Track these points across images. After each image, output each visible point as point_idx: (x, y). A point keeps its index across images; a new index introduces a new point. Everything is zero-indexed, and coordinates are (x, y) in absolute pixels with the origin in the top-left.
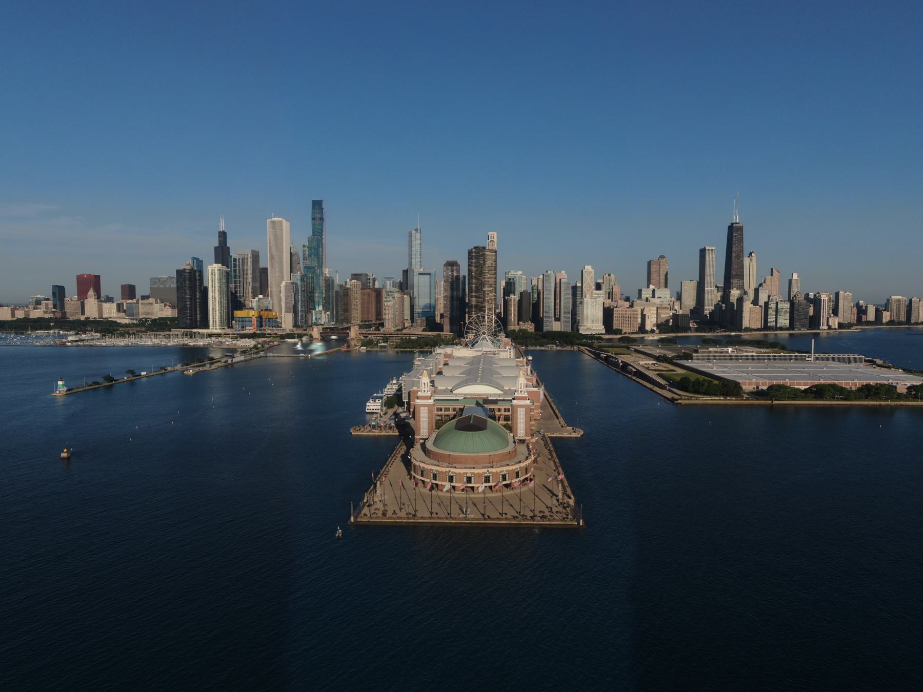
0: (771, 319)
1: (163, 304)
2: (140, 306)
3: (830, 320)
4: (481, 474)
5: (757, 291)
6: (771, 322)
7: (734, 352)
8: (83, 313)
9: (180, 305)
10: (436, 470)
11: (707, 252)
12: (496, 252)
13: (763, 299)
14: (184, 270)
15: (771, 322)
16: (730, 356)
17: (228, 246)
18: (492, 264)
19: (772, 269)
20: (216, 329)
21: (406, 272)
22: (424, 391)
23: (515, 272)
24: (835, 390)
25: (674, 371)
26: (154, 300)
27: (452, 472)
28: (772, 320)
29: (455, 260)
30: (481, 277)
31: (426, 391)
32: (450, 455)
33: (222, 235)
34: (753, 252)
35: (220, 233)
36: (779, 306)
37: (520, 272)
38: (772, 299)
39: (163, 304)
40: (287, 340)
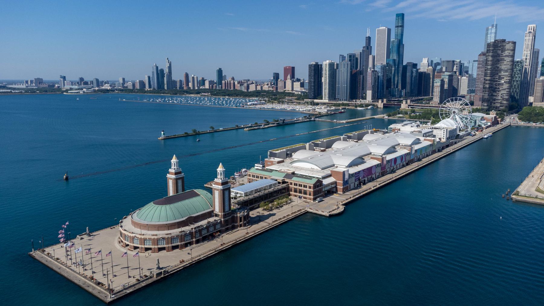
12: (514, 43)
17: (403, 43)
18: (509, 53)
20: (326, 100)
30: (498, 64)
33: (368, 39)
35: (366, 38)
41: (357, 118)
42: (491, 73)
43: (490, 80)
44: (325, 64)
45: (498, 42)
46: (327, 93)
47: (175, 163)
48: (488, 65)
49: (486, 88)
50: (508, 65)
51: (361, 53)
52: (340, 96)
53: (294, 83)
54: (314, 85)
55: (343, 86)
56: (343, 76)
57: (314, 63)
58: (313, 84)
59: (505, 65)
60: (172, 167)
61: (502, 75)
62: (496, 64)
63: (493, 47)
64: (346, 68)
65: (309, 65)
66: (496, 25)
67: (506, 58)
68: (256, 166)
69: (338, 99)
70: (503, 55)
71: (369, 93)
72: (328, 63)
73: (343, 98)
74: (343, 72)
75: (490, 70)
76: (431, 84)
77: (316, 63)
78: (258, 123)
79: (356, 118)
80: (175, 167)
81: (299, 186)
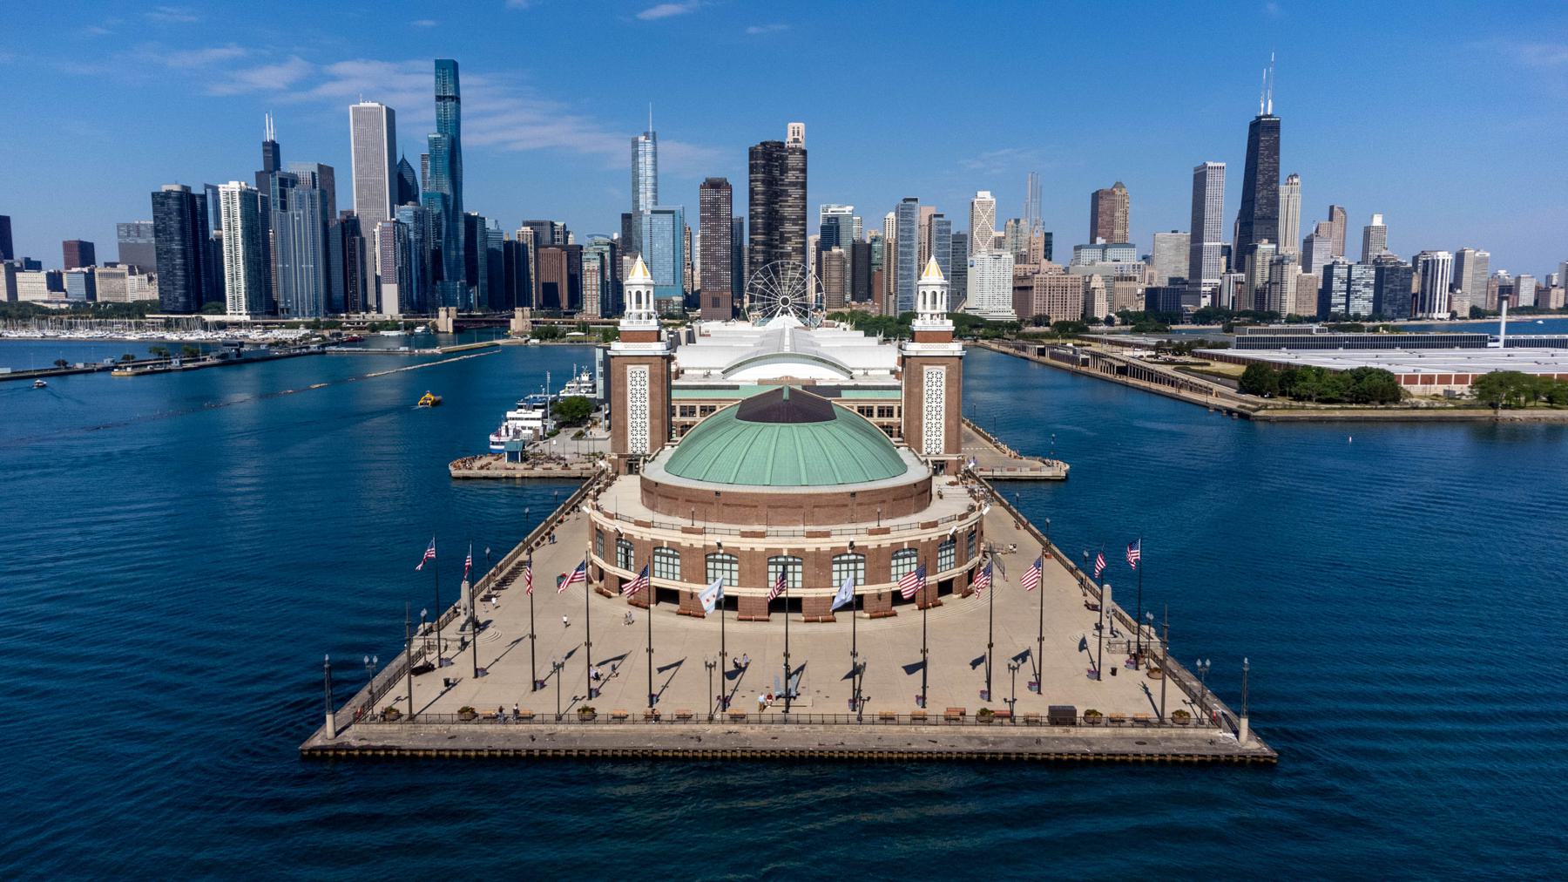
0: (1337, 299)
1: (145, 277)
2: (97, 279)
4: (826, 554)
5: (1308, 244)
6: (1336, 305)
7: (1324, 331)
11: (1209, 172)
12: (804, 153)
13: (1319, 260)
14: (168, 193)
15: (1336, 305)
16: (1315, 339)
18: (797, 178)
19: (1332, 208)
20: (241, 314)
21: (627, 218)
23: (840, 207)
24: (617, 702)
26: (127, 267)
28: (1338, 301)
29: (723, 177)
30: (776, 203)
31: (644, 316)
32: (717, 493)
33: (270, 148)
34: (1296, 176)
36: (1353, 272)
37: (851, 208)
39: (145, 277)
40: (382, 333)
41: (478, 341)
42: (764, 224)
43: (763, 243)
44: (227, 194)
45: (772, 147)
46: (243, 291)
47: (651, 290)
48: (757, 205)
49: (757, 262)
50: (798, 206)
51: (313, 174)
52: (292, 301)
53: (19, 275)
54: (185, 264)
55: (302, 269)
56: (300, 235)
57: (176, 188)
58: (178, 261)
59: (790, 206)
60: (628, 310)
61: (786, 232)
62: (773, 203)
63: (764, 159)
64: (308, 208)
65: (154, 195)
66: (654, 133)
67: (791, 190)
68: (887, 312)
69: (288, 310)
70: (783, 180)
71: (390, 293)
72: (238, 190)
73: (303, 308)
74: (299, 222)
75: (763, 218)
76: (533, 277)
77: (183, 187)
78: (137, 359)
79: (473, 342)
80: (639, 311)
81: (881, 412)
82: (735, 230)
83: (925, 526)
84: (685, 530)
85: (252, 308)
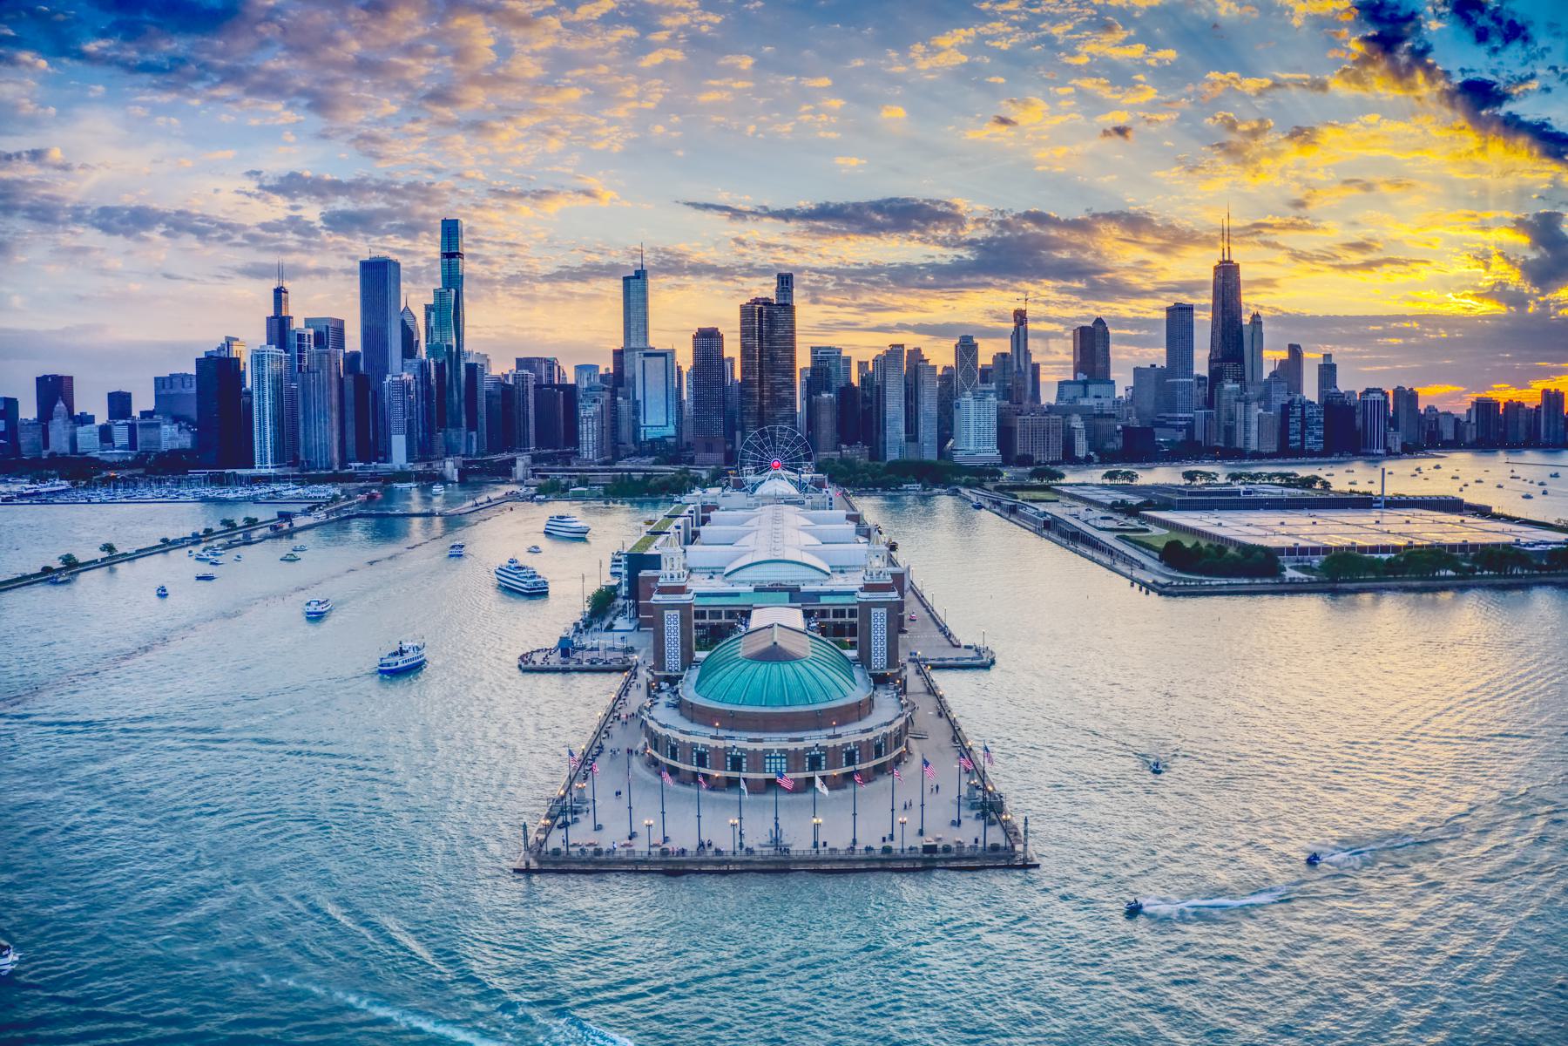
3: (1390, 436)
8: (46, 446)
9: (203, 427)
10: (703, 746)
22: (672, 577)
25: (1147, 531)
27: (739, 750)
38: (102, 549)
39: (176, 426)
40: (395, 485)
71: (399, 443)
82: (411, 402)
83: (863, 732)
84: (712, 737)
85: (279, 459)
